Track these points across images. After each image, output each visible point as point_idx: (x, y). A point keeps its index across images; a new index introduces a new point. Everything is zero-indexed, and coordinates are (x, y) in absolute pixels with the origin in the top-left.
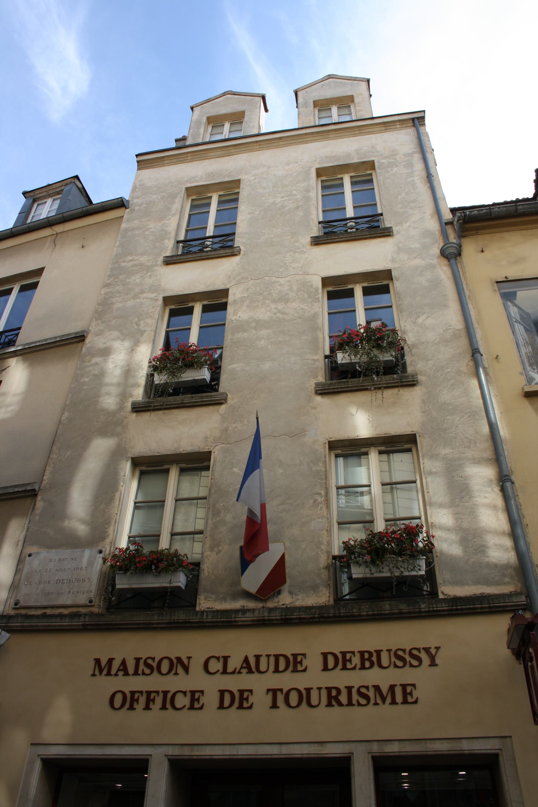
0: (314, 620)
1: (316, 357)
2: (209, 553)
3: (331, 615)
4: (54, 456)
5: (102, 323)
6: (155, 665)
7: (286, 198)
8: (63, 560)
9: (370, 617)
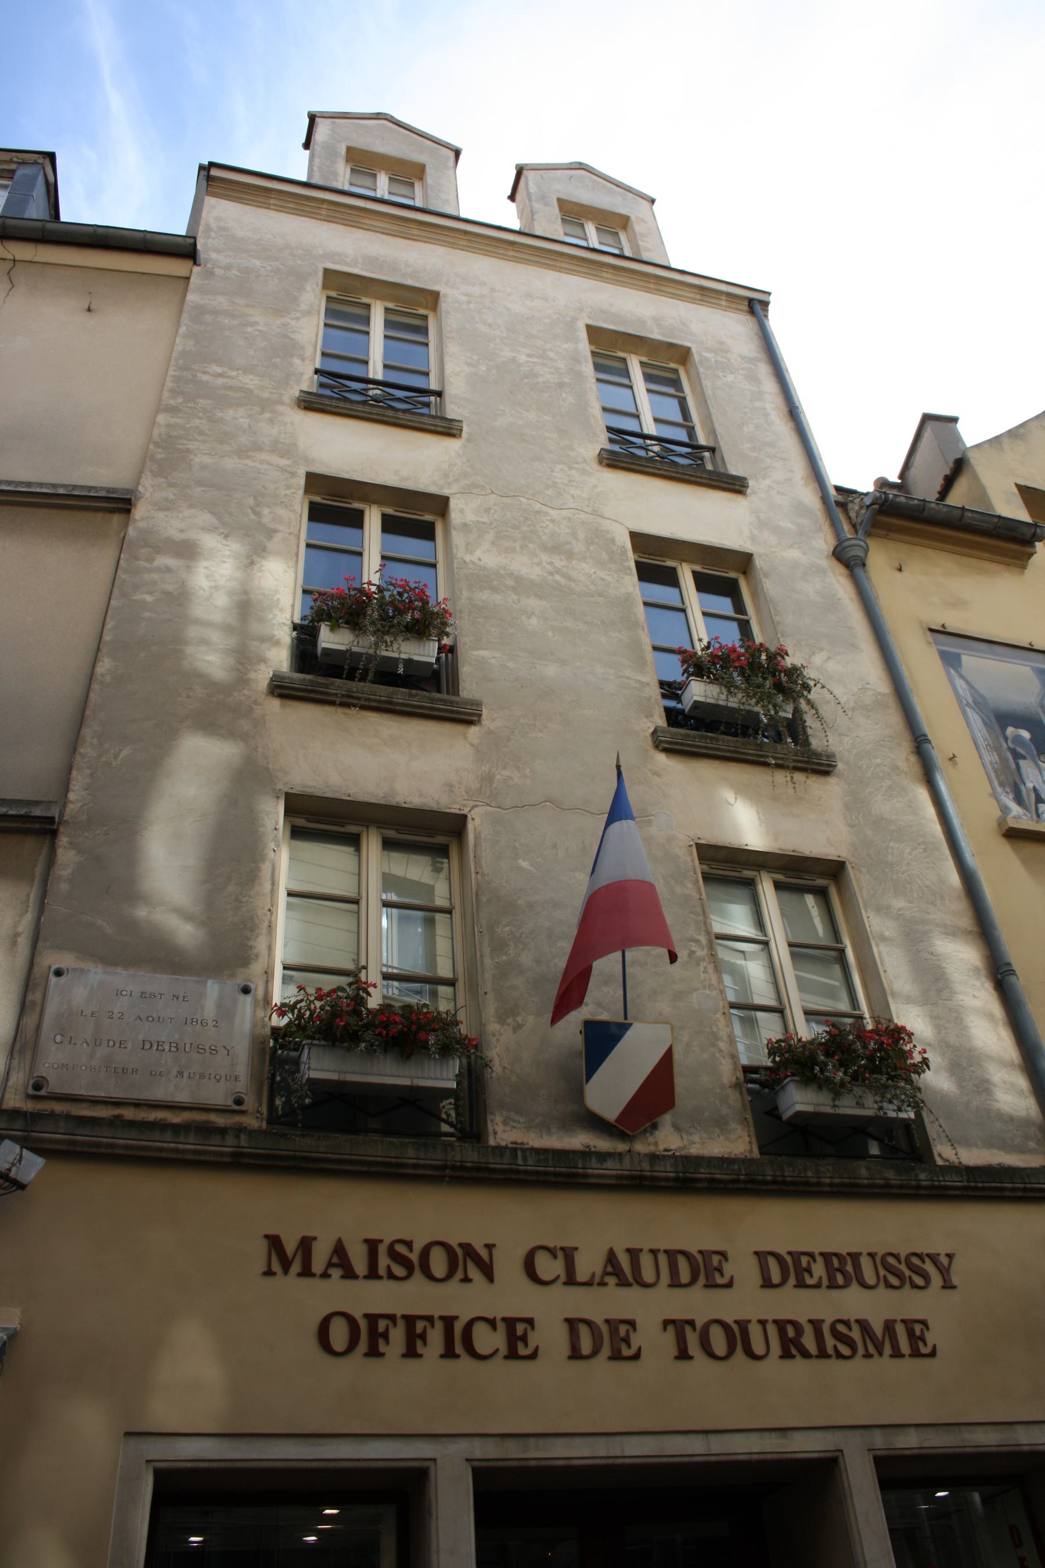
0: (736, 1186)
1: (644, 679)
2: (497, 1027)
3: (769, 1178)
4: (87, 750)
5: (171, 485)
6: (414, 1257)
7: (535, 360)
8: (153, 996)
9: (835, 1189)
